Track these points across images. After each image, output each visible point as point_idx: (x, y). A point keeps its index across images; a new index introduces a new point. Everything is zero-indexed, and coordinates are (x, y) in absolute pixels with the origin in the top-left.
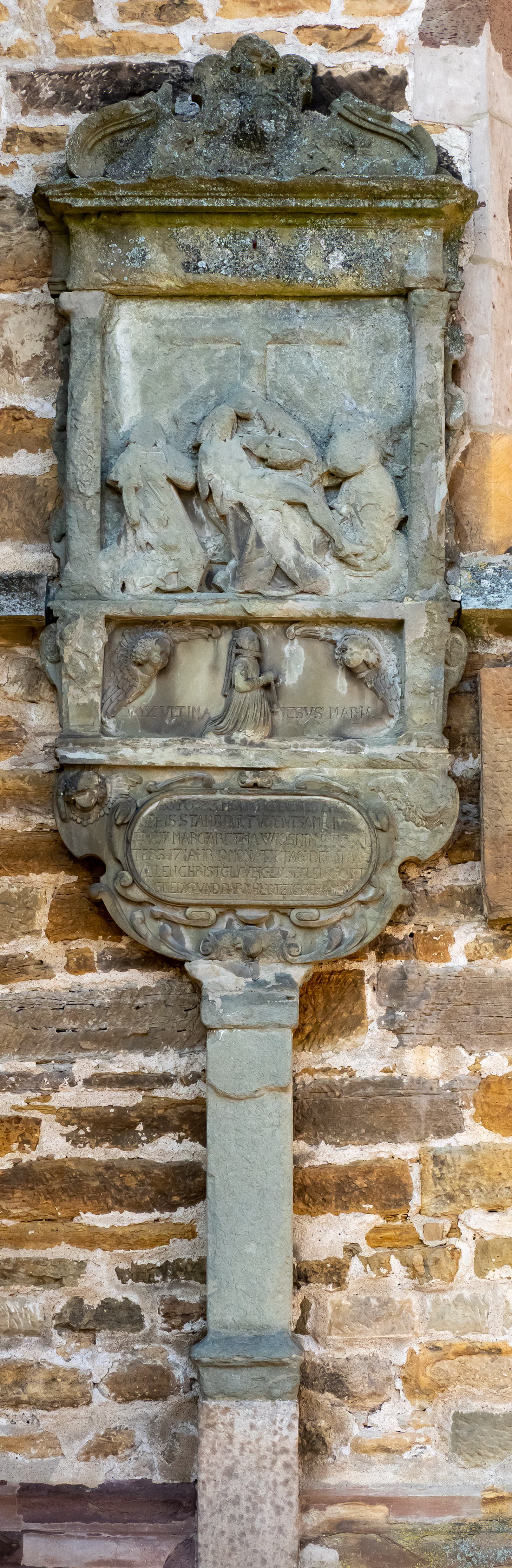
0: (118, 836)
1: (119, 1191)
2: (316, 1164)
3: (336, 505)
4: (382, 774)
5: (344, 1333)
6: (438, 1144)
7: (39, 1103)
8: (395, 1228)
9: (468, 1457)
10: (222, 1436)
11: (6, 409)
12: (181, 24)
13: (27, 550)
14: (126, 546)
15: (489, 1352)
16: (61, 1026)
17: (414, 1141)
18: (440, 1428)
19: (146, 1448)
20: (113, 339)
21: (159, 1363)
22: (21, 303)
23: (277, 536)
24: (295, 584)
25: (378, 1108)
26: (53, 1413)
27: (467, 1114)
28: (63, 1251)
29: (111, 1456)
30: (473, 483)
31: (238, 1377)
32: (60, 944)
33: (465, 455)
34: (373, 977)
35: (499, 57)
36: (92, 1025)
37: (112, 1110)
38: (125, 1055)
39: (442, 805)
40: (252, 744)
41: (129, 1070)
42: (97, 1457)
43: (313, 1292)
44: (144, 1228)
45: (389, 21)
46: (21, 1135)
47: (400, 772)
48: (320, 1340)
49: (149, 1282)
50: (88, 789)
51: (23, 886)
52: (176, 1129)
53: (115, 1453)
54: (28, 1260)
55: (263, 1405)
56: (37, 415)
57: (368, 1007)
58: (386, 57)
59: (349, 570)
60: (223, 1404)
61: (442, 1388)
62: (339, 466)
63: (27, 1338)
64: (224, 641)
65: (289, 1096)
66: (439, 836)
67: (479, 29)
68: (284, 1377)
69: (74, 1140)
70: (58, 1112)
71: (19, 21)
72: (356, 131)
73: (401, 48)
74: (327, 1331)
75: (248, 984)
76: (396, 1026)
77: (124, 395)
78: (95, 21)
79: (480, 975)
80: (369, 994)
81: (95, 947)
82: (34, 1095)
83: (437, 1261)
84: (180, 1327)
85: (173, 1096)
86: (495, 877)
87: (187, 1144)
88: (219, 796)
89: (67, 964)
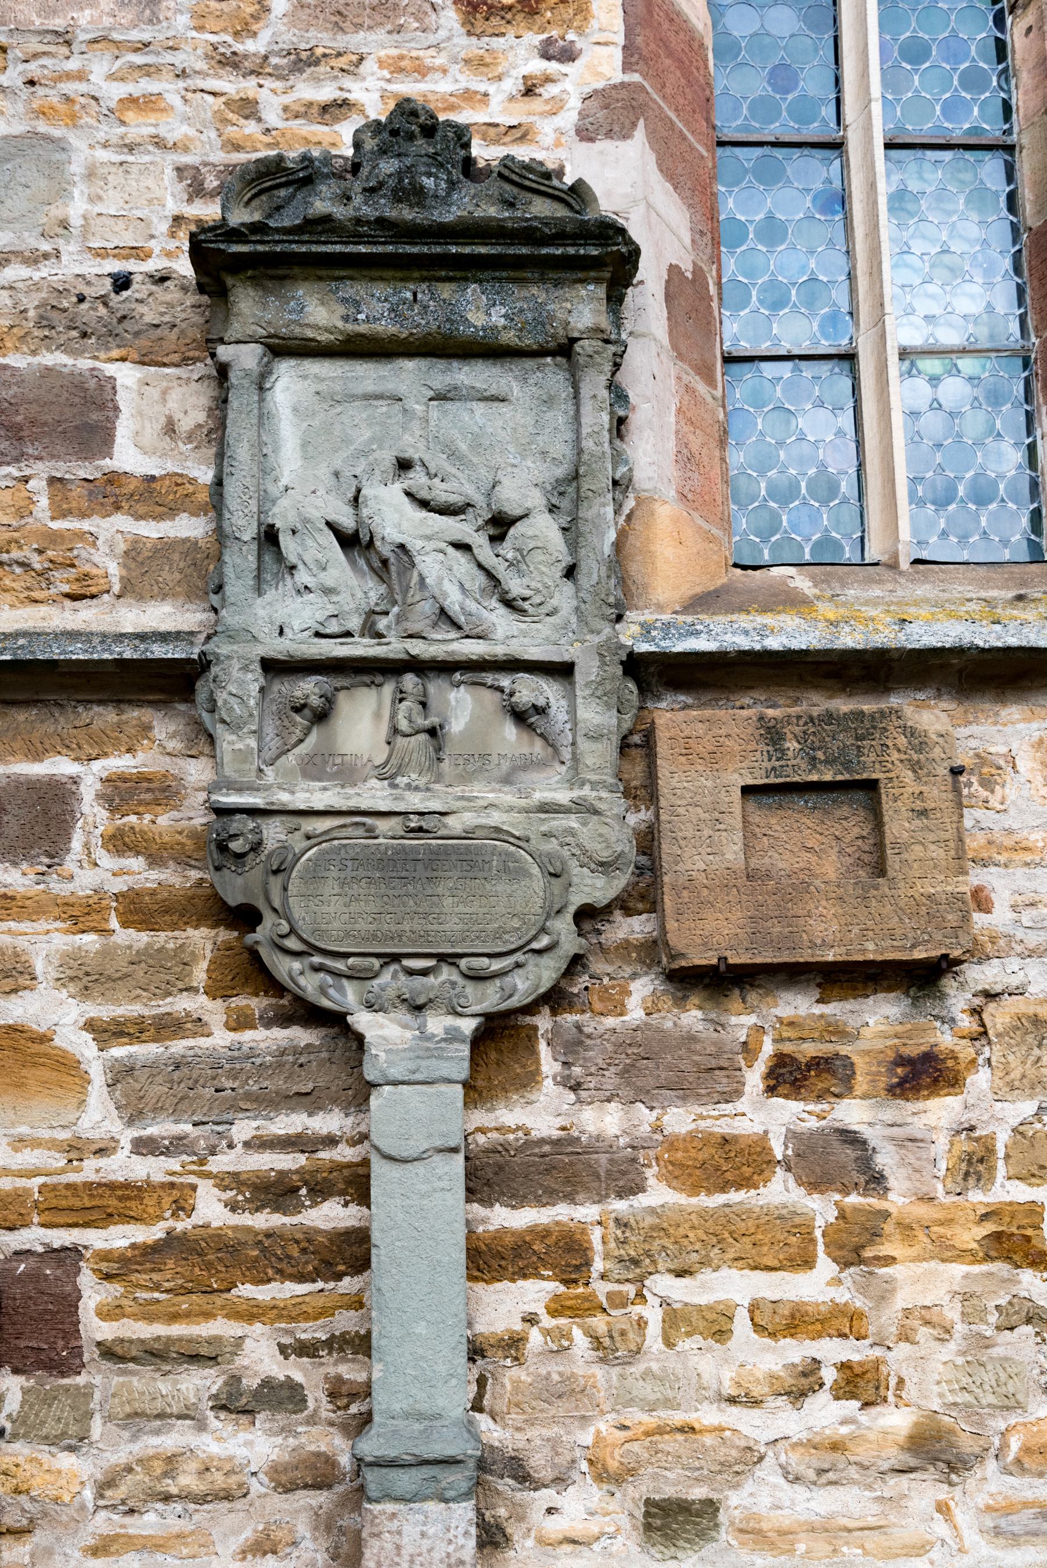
2: (491, 1228)
3: (501, 552)
5: (524, 1412)
6: (620, 1206)
7: (195, 1168)
8: (577, 1297)
9: (662, 1548)
10: (389, 1546)
11: (168, 474)
15: (681, 1430)
16: (219, 1086)
18: (631, 1515)
19: (308, 1544)
21: (323, 1449)
22: (184, 376)
23: (440, 580)
24: (459, 628)
26: (206, 1507)
27: (649, 1173)
28: (220, 1327)
29: (269, 1555)
31: (406, 1477)
32: (219, 1002)
33: (629, 517)
34: (547, 1031)
35: (651, 158)
36: (253, 1087)
38: (287, 1115)
39: (619, 849)
40: (417, 788)
42: (254, 1556)
43: (490, 1367)
44: (307, 1299)
47: (573, 816)
48: (498, 1419)
49: (314, 1356)
50: (242, 834)
51: (180, 942)
52: (342, 1193)
53: (274, 1552)
54: (180, 1339)
55: (433, 1507)
57: (543, 1062)
59: (516, 616)
60: (390, 1507)
61: (632, 1472)
62: (505, 509)
63: (180, 1422)
65: (460, 1159)
66: (616, 882)
67: (634, 125)
68: (459, 1476)
70: (216, 1177)
71: (187, 119)
73: (558, 144)
74: (505, 1409)
75: (415, 1038)
76: (573, 1082)
77: (284, 450)
78: (259, 120)
79: (659, 1030)
81: (257, 1004)
82: (190, 1159)
83: (623, 1333)
84: (347, 1407)
85: (339, 1158)
87: (353, 1209)
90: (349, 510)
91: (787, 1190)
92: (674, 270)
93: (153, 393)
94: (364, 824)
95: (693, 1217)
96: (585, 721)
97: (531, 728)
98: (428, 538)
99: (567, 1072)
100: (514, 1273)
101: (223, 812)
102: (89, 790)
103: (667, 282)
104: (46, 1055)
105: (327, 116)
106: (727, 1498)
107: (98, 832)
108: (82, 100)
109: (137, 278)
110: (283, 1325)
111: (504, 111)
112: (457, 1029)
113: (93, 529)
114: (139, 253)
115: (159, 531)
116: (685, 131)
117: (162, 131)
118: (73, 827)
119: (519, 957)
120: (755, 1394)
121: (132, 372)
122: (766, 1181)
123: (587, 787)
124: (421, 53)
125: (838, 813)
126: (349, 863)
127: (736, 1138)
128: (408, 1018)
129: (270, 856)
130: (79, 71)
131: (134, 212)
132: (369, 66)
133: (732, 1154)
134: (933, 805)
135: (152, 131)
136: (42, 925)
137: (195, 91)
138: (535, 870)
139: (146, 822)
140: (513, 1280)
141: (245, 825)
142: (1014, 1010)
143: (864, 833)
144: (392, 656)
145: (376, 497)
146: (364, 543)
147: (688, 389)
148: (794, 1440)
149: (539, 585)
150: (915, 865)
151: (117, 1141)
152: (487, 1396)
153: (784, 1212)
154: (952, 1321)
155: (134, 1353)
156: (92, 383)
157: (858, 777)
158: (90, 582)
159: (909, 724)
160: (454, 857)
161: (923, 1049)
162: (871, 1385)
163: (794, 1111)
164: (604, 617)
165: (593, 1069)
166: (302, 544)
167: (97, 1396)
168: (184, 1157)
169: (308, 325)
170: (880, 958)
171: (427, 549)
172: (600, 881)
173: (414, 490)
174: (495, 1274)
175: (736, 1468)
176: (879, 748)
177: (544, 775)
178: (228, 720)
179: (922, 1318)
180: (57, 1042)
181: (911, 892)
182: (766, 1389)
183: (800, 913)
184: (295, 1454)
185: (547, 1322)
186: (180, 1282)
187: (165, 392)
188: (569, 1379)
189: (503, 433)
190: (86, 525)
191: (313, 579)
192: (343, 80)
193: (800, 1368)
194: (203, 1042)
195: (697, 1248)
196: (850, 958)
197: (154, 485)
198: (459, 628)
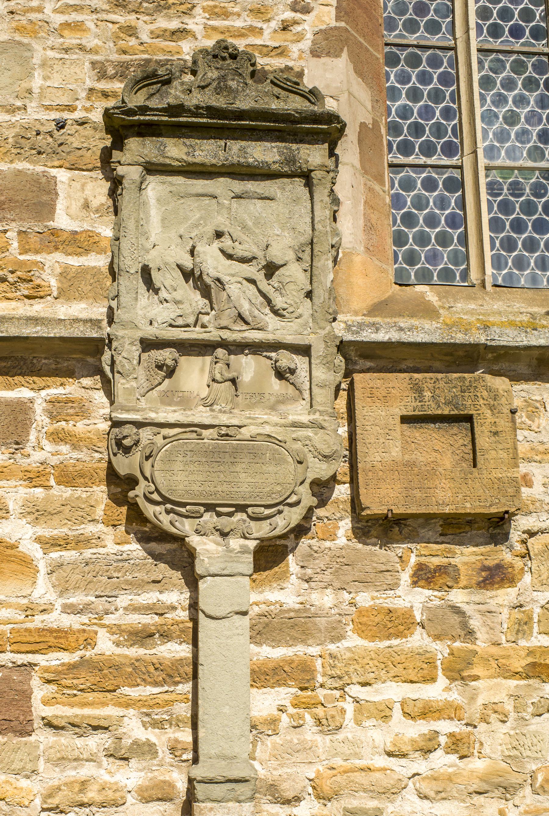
3: (271, 283)
6: (332, 647)
8: (308, 697)
12: (184, 41)
17: (318, 645)
21: (167, 779)
24: (247, 323)
28: (111, 711)
35: (351, 67)
39: (335, 449)
40: (225, 412)
41: (150, 602)
52: (179, 637)
54: (89, 717)
59: (277, 318)
62: (274, 261)
66: (333, 466)
67: (342, 50)
70: (108, 627)
71: (97, 36)
73: (300, 58)
76: (307, 577)
78: (137, 38)
83: (333, 717)
88: (205, 441)
90: (188, 256)
91: (423, 639)
92: (363, 125)
93: (77, 185)
94: (196, 432)
95: (372, 653)
96: (317, 377)
97: (287, 380)
98: (233, 275)
99: (304, 572)
100: (273, 683)
101: (116, 424)
102: (39, 407)
103: (359, 133)
104: (15, 556)
105: (174, 37)
106: (387, 807)
107: (44, 431)
108: (40, 23)
109: (69, 122)
110: (145, 710)
111: (271, 39)
112: (246, 546)
113: (42, 260)
114: (71, 108)
115: (79, 262)
116: (368, 47)
117: (84, 42)
118: (30, 428)
119: (281, 507)
120: (403, 750)
121: (65, 174)
122: (412, 634)
123: (318, 414)
124: (226, 5)
125: (452, 432)
126: (188, 453)
127: (396, 610)
128: (219, 539)
129: (144, 448)
130: (38, 7)
131: (68, 86)
132: (198, 10)
133: (393, 619)
134: (501, 429)
135: (78, 41)
136: (12, 483)
137: (102, 21)
138: (290, 459)
139: (70, 425)
140: (273, 687)
141: (132, 431)
142: (544, 541)
143: (465, 443)
144: (212, 339)
145: (204, 252)
146: (196, 276)
147: (371, 190)
148: (424, 775)
149: (292, 302)
150: (492, 461)
151: (54, 605)
152: (258, 751)
153: (421, 651)
154: (509, 710)
155: (63, 724)
156: (44, 180)
157: (462, 413)
158: (40, 289)
159: (489, 384)
160: (246, 451)
161: (496, 562)
162: (466, 745)
163: (427, 595)
164: (327, 320)
165: (318, 570)
166: (164, 276)
167: (42, 747)
168: (90, 615)
169: (167, 157)
170: (473, 512)
171: (232, 281)
172: (324, 466)
173: (225, 249)
174: (262, 684)
175: (392, 791)
176: (473, 397)
177: (294, 406)
178: (122, 372)
179: (493, 709)
180: (21, 548)
181: (489, 476)
182: (409, 748)
183: (431, 486)
184: (151, 781)
185: (291, 710)
186: (89, 685)
187: (83, 186)
188: (303, 742)
189: (272, 217)
190: (38, 258)
191: (169, 295)
192: (183, 18)
193: (428, 736)
194: (101, 550)
195: (373, 670)
196: (457, 512)
197: (77, 237)
198: (247, 323)
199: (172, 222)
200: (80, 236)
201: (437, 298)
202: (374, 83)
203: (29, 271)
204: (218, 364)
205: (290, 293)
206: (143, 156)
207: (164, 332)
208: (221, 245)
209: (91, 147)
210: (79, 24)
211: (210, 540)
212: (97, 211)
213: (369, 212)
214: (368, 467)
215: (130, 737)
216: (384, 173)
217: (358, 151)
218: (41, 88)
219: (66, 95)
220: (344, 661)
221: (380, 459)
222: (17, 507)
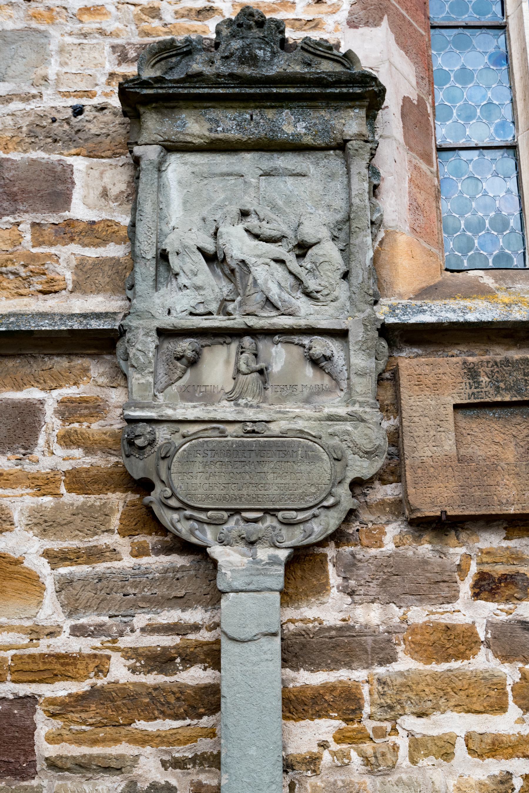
0: (163, 465)
1: (163, 705)
2: (298, 685)
3: (303, 264)
4: (337, 424)
6: (380, 670)
7: (109, 645)
8: (353, 730)
11: (103, 220)
12: (210, 20)
13: (113, 299)
14: (171, 289)
16: (126, 592)
17: (364, 668)
20: (166, 175)
23: (266, 281)
24: (278, 309)
25: (338, 645)
27: (399, 649)
30: (387, 258)
32: (127, 538)
33: (381, 243)
34: (333, 557)
36: (147, 593)
37: (159, 649)
38: (168, 611)
39: (377, 443)
40: (251, 406)
41: (171, 621)
43: (297, 777)
44: (180, 731)
45: (329, 17)
46: (97, 667)
47: (348, 423)
50: (143, 435)
51: (103, 501)
52: (203, 662)
54: (98, 756)
56: (121, 224)
57: (330, 577)
58: (328, 35)
59: (313, 302)
64: (234, 346)
65: (278, 640)
66: (376, 463)
67: (381, 19)
69: (133, 670)
70: (122, 651)
71: (118, 19)
72: (311, 57)
73: (336, 30)
77: (172, 206)
78: (161, 19)
79: (404, 557)
80: (331, 568)
82: (107, 639)
83: (383, 755)
85: (201, 639)
86: (414, 490)
87: (210, 672)
88: (229, 438)
89: (131, 552)
90: (212, 240)
91: (488, 661)
92: (406, 99)
93: (95, 173)
94: (218, 428)
95: (428, 678)
96: (355, 365)
97: (322, 369)
98: (259, 256)
99: (346, 584)
100: (313, 715)
102: (50, 408)
104: (18, 573)
105: (200, 16)
107: (55, 433)
108: (58, 9)
109: (87, 108)
110: (164, 748)
111: (305, 12)
112: (276, 557)
113: (57, 253)
115: (96, 253)
116: (412, 21)
117: (104, 26)
118: (39, 431)
119: (315, 511)
121: (83, 162)
122: (475, 655)
123: (357, 405)
125: (514, 421)
126: (209, 453)
127: (454, 627)
128: (245, 549)
129: (160, 448)
131: (86, 71)
133: (452, 637)
135: (98, 26)
136: (19, 491)
137: (123, 4)
138: (325, 457)
139: (84, 427)
140: (312, 719)
141: (145, 429)
144: (236, 326)
145: (227, 233)
147: (415, 167)
149: (327, 284)
151: (61, 628)
153: (486, 675)
156: (59, 168)
158: (54, 284)
160: (274, 449)
163: (491, 609)
164: (366, 302)
165: (362, 582)
166: (183, 261)
168: (103, 638)
171: (259, 263)
172: (366, 463)
173: (250, 229)
174: (300, 715)
177: (331, 397)
178: (136, 365)
180: (26, 564)
183: (492, 483)
185: (334, 747)
187: (102, 173)
188: (348, 784)
189: (305, 195)
190: (53, 250)
195: (430, 698)
196: (524, 512)
197: (94, 227)
198: (278, 309)
199: (194, 205)
200: (97, 226)
201: (493, 281)
202: (419, 59)
203: (43, 265)
204: (244, 354)
205: (324, 274)
206: (162, 134)
207: (183, 322)
208: (246, 225)
209: (111, 132)
210: (99, 8)
211: (235, 551)
212: (116, 199)
213: (415, 190)
214: (416, 463)
215: (146, 780)
216: (431, 153)
217: (401, 125)
218: (57, 75)
219: (84, 81)
220: (395, 688)
221: (431, 454)
222: (23, 518)
